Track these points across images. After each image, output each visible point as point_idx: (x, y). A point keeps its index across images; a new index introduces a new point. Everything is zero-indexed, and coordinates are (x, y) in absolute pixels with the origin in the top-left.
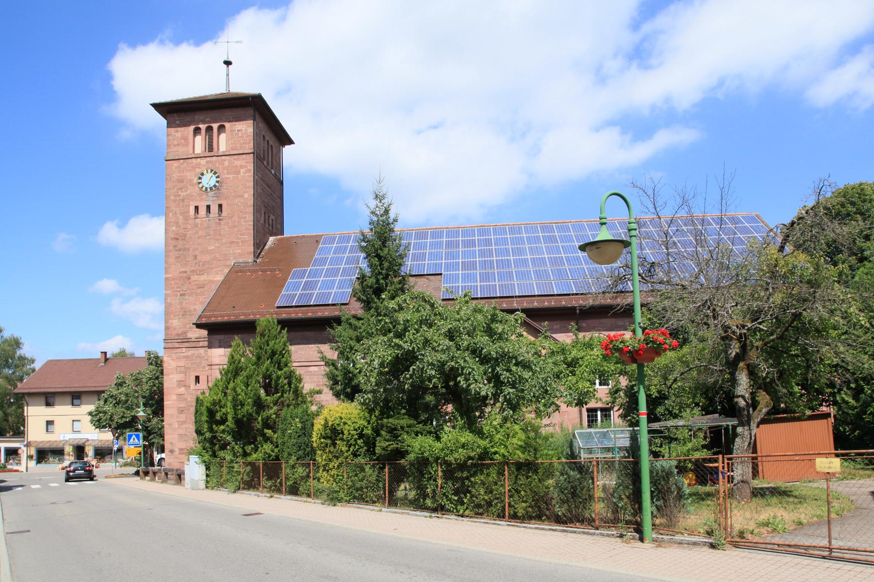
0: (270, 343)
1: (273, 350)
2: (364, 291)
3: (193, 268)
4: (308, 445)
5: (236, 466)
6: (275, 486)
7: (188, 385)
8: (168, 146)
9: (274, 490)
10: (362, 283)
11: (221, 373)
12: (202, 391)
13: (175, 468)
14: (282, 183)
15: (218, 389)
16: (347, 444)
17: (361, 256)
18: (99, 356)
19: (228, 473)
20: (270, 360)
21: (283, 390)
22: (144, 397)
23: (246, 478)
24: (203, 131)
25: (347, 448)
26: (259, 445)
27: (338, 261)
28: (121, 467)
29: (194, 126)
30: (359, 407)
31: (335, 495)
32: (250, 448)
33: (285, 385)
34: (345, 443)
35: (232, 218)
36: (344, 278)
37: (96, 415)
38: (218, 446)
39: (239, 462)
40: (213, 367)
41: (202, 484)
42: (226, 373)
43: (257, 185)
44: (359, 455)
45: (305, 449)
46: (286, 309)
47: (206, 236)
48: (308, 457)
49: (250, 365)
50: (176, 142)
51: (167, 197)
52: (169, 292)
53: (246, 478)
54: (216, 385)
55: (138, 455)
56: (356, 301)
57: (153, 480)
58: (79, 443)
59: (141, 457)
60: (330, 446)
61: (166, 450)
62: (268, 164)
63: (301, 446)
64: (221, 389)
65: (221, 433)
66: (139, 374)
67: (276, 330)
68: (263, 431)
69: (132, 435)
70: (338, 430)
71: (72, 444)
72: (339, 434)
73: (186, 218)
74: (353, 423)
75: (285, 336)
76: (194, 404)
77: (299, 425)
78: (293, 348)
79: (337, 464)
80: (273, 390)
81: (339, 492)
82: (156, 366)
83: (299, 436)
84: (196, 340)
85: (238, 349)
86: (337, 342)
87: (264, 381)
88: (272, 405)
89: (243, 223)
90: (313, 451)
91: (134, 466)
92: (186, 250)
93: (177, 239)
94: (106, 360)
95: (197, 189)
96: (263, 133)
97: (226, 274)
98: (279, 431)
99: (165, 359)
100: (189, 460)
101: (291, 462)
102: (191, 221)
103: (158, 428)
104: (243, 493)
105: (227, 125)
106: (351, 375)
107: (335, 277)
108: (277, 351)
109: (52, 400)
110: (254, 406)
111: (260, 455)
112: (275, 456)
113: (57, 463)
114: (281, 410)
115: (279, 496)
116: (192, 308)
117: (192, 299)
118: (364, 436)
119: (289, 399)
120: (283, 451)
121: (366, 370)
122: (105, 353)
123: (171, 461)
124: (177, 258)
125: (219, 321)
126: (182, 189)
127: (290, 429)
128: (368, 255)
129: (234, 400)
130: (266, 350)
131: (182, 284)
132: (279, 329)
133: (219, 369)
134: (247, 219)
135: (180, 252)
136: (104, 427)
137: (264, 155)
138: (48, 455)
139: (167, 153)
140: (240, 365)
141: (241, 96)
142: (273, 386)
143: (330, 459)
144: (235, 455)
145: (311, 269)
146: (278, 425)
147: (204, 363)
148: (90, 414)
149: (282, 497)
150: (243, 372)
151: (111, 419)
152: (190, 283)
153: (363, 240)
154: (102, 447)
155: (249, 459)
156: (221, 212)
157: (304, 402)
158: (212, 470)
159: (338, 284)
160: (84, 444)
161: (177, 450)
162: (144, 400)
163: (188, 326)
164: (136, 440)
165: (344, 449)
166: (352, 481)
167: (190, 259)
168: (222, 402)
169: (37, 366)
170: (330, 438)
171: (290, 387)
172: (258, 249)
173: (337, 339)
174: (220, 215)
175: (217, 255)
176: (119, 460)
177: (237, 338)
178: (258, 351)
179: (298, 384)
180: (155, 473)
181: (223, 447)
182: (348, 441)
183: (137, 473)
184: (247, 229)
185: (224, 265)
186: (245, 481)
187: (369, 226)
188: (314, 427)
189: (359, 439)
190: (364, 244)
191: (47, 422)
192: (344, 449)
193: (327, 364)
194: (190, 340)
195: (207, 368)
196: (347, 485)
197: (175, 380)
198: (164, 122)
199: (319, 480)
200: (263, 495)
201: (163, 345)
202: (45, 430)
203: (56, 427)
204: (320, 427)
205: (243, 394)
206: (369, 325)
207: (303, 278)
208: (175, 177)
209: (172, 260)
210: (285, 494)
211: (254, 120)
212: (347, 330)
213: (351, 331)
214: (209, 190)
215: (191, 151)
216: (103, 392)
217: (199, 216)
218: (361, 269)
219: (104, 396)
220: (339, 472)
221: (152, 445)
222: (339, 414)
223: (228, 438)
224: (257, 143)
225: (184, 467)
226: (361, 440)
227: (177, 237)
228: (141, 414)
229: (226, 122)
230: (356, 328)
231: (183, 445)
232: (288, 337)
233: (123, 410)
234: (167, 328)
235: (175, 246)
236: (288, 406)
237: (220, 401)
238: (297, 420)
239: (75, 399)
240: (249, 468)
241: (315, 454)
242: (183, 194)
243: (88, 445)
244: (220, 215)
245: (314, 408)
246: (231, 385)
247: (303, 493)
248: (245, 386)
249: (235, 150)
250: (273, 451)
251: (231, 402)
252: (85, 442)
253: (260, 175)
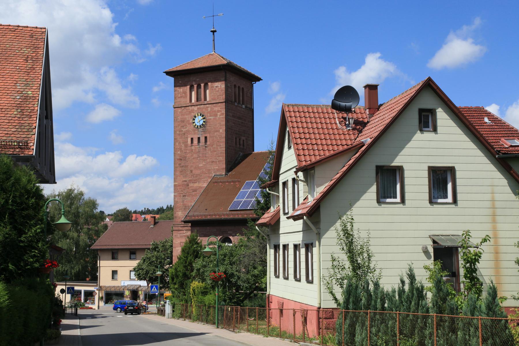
35: (213, 145)
50: (179, 96)
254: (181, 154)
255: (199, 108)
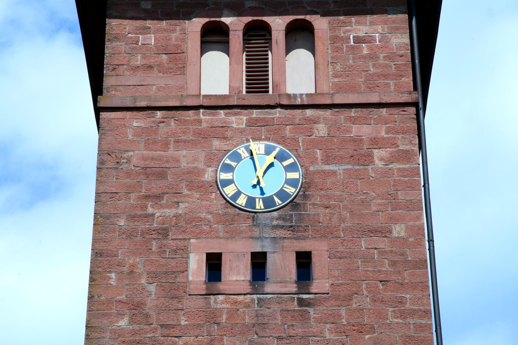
29: (204, 20)
35: (348, 299)
50: (138, 60)
126: (159, 197)
208: (134, 161)
229: (315, 13)
254: (134, 333)
255: (257, 120)
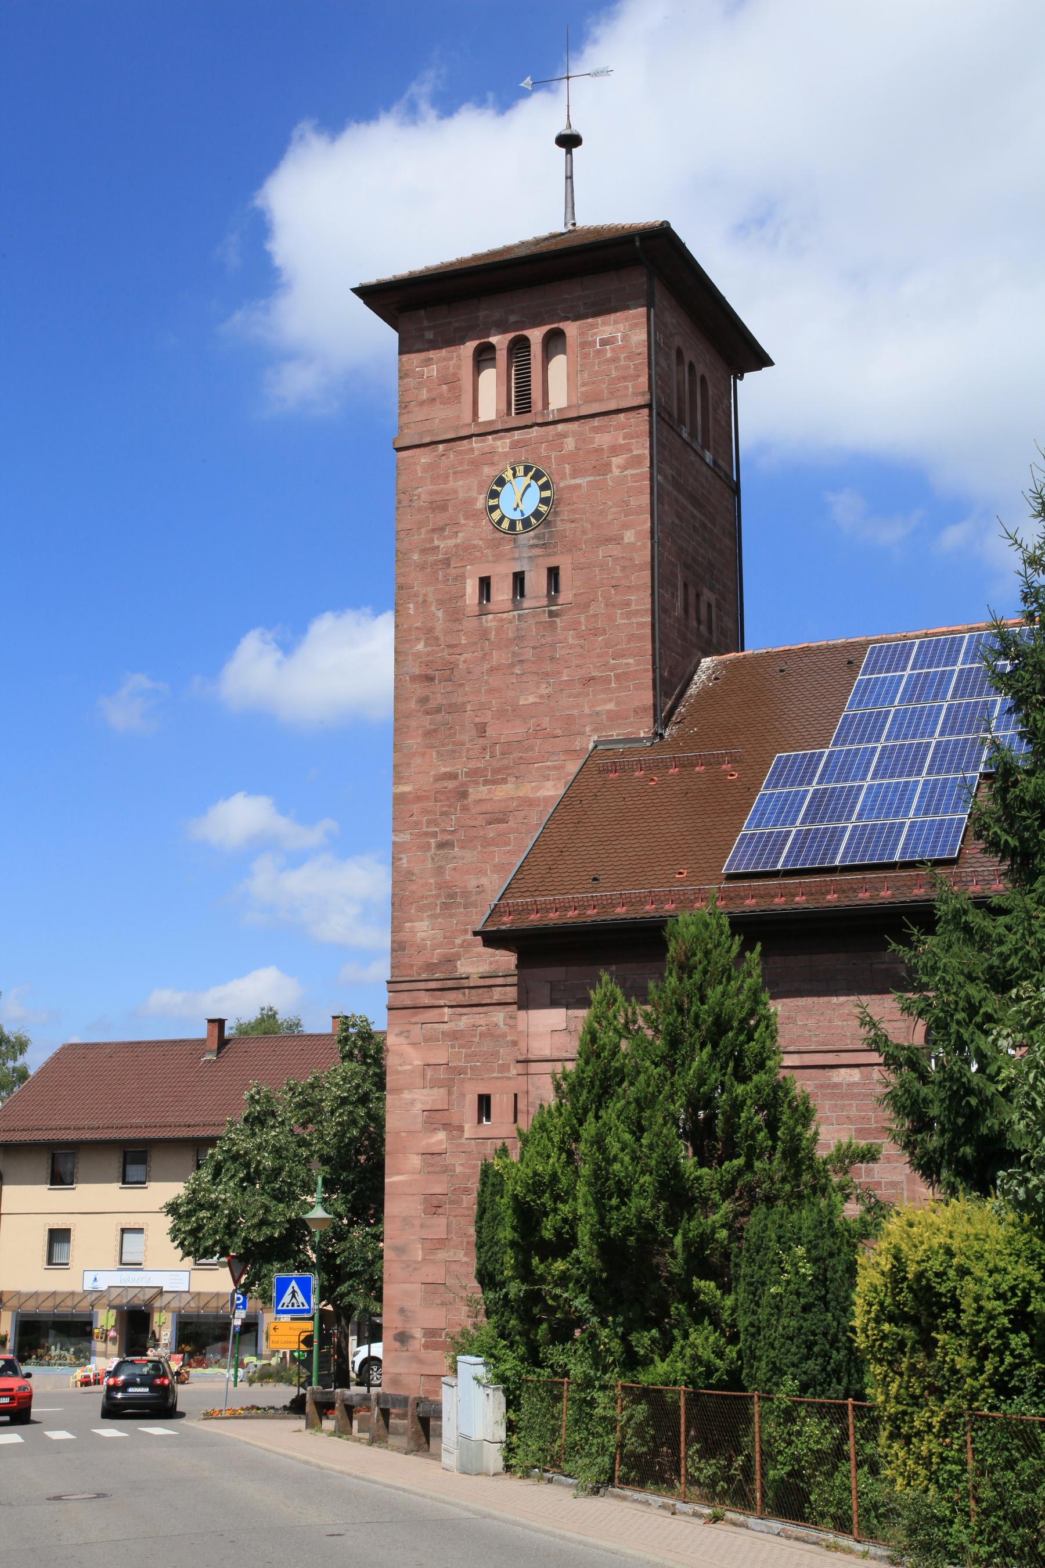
0: (709, 992)
1: (718, 1017)
2: (1009, 816)
3: (473, 764)
4: (835, 1340)
5: (601, 1397)
6: (729, 1479)
7: (455, 1122)
8: (404, 406)
9: (725, 1493)
10: (1004, 791)
11: (558, 1087)
12: (499, 1143)
13: (413, 1395)
14: (735, 489)
15: (550, 1139)
16: (974, 1345)
17: (994, 702)
18: (201, 1031)
19: (577, 1421)
20: (708, 1048)
21: (751, 1148)
22: (325, 1160)
23: (633, 1444)
24: (502, 356)
25: (973, 1362)
26: (676, 1332)
27: (923, 722)
28: (251, 1382)
30: (1012, 1217)
31: (938, 1533)
32: (647, 1342)
33: (759, 1129)
34: (966, 1342)
35: (587, 606)
36: (903, 780)
37: (189, 1214)
38: (545, 1326)
39: (612, 1388)
40: (534, 1067)
41: (494, 1458)
42: (572, 1089)
43: (660, 501)
44: (1019, 1391)
45: (826, 1356)
46: (755, 883)
47: (512, 665)
48: (839, 1382)
49: (648, 1063)
50: (424, 395)
51: (400, 557)
52: (405, 837)
53: (633, 1444)
54: (543, 1127)
55: (303, 1347)
56: (985, 851)
57: (344, 1431)
58: (136, 1302)
59: (310, 1353)
60: (913, 1350)
61: (386, 1334)
62: (693, 434)
63: (815, 1343)
64: (556, 1139)
65: (556, 1285)
66: (312, 1086)
67: (729, 951)
68: (690, 1283)
69: (289, 1280)
70: (941, 1295)
71: (116, 1302)
72: (944, 1308)
73: (455, 615)
74: (991, 1273)
75: (757, 971)
76: (475, 1185)
77: (807, 1269)
78: (777, 1007)
79: (941, 1416)
80: (720, 1145)
81: (951, 1522)
82: (364, 1063)
83: (806, 1309)
84: (482, 982)
85: (610, 1014)
86: (922, 987)
87: (692, 1117)
88: (716, 1196)
89: (620, 621)
90: (856, 1363)
91: (289, 1382)
92: (455, 709)
93: (430, 679)
94: (223, 1043)
95: (485, 526)
96: (678, 341)
97: (572, 778)
98: (742, 1286)
99: (391, 1041)
100: (455, 1371)
101: (783, 1397)
102: (470, 624)
103: (365, 1259)
104: (624, 1498)
105: (571, 329)
106: (974, 1101)
107: (909, 775)
108: (731, 1019)
109: (69, 1165)
110: (659, 1197)
111: (680, 1365)
112: (728, 1372)
113: (71, 1365)
114: (746, 1213)
115: (742, 1518)
116: (472, 883)
117: (470, 856)
118: (1034, 1323)
119: (771, 1179)
120: (755, 1358)
121: (1033, 1087)
122: (221, 1023)
123: (401, 1368)
124: (428, 734)
125: (551, 923)
127: (777, 1282)
128: (1020, 702)
129: (599, 1175)
130: (697, 1016)
131: (442, 814)
132: (735, 949)
133: (554, 1075)
134: (633, 607)
135: (439, 717)
136: (208, 1253)
137: (681, 410)
138: (47, 1336)
139: (401, 428)
140: (615, 1064)
141: (611, 236)
142: (719, 1132)
143: (913, 1397)
144: (598, 1361)
145: (831, 754)
146: (737, 1265)
147: (506, 1054)
148: (172, 1209)
149: (752, 1521)
150: (625, 1084)
151: (230, 1230)
152: (465, 809)
153: (1004, 653)
154: (199, 1316)
155: (645, 1378)
156: (557, 591)
157: (820, 1189)
158: (526, 1407)
159: (921, 797)
160: (149, 1304)
161: (418, 1333)
162: (327, 1168)
163: (458, 941)
164: (300, 1298)
165: (963, 1362)
166: (995, 1486)
167: (466, 738)
168: (559, 1181)
169: (34, 1060)
170: (913, 1320)
171: (774, 1138)
172: (668, 695)
173: (925, 979)
174: (552, 600)
175: (546, 722)
176: (247, 1359)
177: (606, 977)
178: (671, 1019)
179: (799, 1129)
180: (350, 1410)
181: (562, 1334)
182: (977, 1336)
183: (297, 1407)
184: (631, 638)
185: (567, 752)
186: (632, 1453)
187: (1022, 606)
188: (858, 1280)
189: (1016, 1331)
190: (1006, 665)
191: (52, 1232)
192: (963, 1362)
193: (892, 1061)
194: (465, 983)
195: (514, 1072)
196: (978, 1501)
197: (418, 1107)
198: (390, 336)
199: (874, 1470)
200: (688, 1508)
201: (384, 997)
202: (45, 1258)
203: (77, 1249)
204: (879, 1280)
205: (627, 1159)
206: (1032, 934)
207: (809, 783)
209: (414, 742)
210: (763, 1511)
211: (650, 305)
212: (955, 949)
213: (969, 952)
214: (519, 527)
215: (468, 417)
216: (211, 1141)
217: (491, 607)
218: (996, 746)
219: (212, 1156)
220: (949, 1446)
221: (344, 1312)
222: (941, 1239)
223: (576, 1303)
224: (657, 374)
225: (437, 1393)
226: (1024, 1335)
227: (430, 672)
228: (318, 1213)
229: (566, 319)
230: (984, 942)
231: (433, 1317)
232: (763, 975)
233: (265, 1199)
234: (398, 947)
235: (424, 700)
236: (770, 1200)
237: (554, 1178)
238: (800, 1251)
239: (133, 1163)
240: (641, 1410)
241: (861, 1372)
242: (444, 544)
243: (161, 1309)
244: (552, 600)
245: (852, 1210)
246: (589, 1129)
247: (822, 1515)
248: (633, 1133)
249: (596, 400)
250: (720, 1355)
251: (589, 1184)
252: (153, 1298)
253: (669, 472)
